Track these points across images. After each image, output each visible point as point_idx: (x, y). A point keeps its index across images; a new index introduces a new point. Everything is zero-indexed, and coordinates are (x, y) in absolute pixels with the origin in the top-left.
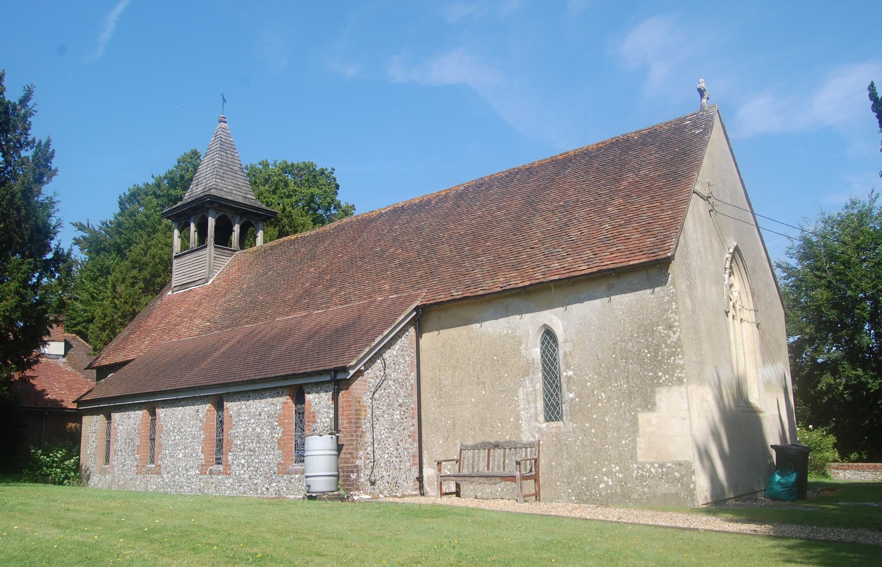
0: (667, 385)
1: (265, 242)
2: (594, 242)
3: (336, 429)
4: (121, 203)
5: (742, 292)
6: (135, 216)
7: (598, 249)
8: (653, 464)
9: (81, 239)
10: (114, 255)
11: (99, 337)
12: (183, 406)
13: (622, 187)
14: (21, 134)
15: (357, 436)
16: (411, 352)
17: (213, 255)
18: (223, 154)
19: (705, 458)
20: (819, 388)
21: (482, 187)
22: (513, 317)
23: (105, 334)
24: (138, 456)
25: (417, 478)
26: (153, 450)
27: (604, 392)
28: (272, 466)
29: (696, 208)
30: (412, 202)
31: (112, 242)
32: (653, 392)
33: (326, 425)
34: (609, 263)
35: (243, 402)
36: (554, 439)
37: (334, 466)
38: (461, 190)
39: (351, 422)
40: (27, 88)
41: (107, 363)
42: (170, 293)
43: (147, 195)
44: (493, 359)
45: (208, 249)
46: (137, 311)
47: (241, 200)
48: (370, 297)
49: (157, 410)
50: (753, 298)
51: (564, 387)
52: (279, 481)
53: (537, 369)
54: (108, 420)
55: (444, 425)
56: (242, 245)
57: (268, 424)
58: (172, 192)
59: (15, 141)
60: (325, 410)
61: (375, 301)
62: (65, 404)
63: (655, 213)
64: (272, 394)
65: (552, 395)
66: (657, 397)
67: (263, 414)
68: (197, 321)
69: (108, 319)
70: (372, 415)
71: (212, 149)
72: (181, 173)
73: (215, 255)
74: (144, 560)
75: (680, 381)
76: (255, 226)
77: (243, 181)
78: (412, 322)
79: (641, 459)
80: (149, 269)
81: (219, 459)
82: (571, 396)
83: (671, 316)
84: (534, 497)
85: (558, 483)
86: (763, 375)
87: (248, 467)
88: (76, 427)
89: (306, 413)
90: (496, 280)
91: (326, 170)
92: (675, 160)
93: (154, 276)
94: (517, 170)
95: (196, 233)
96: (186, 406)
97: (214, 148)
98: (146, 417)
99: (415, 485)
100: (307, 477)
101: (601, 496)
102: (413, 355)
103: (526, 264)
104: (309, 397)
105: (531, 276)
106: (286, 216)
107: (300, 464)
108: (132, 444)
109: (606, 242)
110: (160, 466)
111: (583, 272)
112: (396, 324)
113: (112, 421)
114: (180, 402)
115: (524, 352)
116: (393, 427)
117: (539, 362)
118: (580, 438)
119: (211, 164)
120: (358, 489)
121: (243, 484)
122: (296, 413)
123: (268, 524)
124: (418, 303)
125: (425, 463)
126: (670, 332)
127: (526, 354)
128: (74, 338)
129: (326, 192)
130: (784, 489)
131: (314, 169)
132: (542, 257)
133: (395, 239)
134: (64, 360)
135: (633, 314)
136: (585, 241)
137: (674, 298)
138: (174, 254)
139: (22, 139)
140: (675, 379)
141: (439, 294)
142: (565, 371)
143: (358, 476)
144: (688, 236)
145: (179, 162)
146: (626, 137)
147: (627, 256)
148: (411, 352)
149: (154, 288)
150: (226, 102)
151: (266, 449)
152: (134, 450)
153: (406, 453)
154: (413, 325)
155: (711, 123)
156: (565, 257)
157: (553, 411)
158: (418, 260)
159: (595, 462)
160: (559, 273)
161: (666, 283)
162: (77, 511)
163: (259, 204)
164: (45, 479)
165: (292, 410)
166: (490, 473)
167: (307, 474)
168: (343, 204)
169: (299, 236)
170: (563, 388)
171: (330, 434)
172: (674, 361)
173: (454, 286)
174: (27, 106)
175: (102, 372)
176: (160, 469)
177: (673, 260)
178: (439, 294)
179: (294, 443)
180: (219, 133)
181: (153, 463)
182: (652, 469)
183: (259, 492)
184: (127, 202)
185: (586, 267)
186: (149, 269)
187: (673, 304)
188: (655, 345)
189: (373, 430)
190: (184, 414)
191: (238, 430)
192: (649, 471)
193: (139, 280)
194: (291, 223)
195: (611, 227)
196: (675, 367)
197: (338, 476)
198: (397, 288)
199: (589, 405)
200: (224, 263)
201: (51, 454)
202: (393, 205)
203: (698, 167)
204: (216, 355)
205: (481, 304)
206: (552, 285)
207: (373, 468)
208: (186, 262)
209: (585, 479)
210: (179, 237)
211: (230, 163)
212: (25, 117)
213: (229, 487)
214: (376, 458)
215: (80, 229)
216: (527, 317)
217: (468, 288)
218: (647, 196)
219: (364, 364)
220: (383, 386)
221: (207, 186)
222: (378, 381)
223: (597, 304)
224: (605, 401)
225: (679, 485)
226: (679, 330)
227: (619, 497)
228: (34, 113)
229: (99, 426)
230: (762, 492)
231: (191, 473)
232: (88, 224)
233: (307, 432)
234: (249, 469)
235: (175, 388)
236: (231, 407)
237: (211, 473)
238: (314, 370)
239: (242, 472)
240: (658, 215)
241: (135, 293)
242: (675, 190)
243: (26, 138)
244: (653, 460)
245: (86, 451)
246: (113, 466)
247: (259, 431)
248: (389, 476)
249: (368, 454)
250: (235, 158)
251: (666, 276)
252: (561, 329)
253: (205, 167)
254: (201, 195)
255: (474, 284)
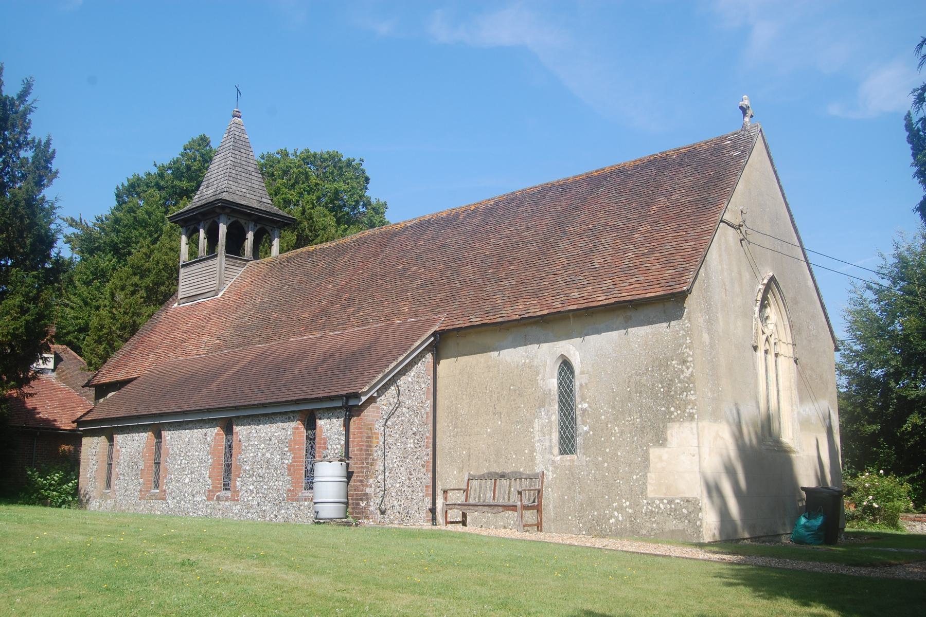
0: (679, 421)
1: (281, 251)
2: (616, 271)
3: (346, 456)
4: (118, 196)
5: (778, 324)
6: (134, 212)
7: (618, 279)
8: (662, 500)
9: (73, 236)
10: (109, 256)
11: (95, 351)
12: (190, 429)
13: (652, 212)
14: (20, 133)
15: (367, 463)
16: (427, 379)
17: (224, 265)
18: (236, 152)
19: (715, 494)
20: (904, 429)
21: (513, 202)
22: (531, 346)
23: (102, 347)
24: (141, 481)
25: (429, 509)
26: (158, 474)
27: (618, 426)
28: (281, 492)
29: (724, 238)
30: (439, 215)
31: (108, 240)
32: (665, 427)
33: (336, 452)
34: (626, 294)
35: (253, 427)
36: (567, 472)
37: (343, 493)
38: (491, 205)
39: (361, 450)
40: (26, 82)
41: (108, 381)
42: (176, 305)
43: (148, 187)
44: (510, 389)
45: (218, 258)
46: (138, 322)
47: (255, 205)
48: (389, 320)
49: (162, 432)
50: (791, 331)
51: (579, 419)
52: (288, 508)
53: (553, 400)
54: (109, 442)
55: (460, 455)
56: (256, 255)
57: (278, 449)
58: (177, 183)
59: (13, 140)
60: (336, 436)
61: (393, 324)
62: (58, 424)
63: (679, 242)
64: (283, 419)
65: (567, 428)
66: (669, 432)
67: (273, 439)
68: (206, 339)
69: (105, 331)
70: (384, 443)
71: (225, 146)
72: (187, 163)
73: (226, 266)
74: (166, 555)
75: (691, 417)
76: (270, 232)
77: (258, 183)
78: (429, 348)
79: (651, 495)
80: (152, 277)
81: (226, 484)
82: (585, 428)
83: (685, 350)
84: (536, 527)
85: (570, 518)
86: (799, 413)
87: (257, 493)
88: (69, 450)
89: (317, 440)
90: (516, 307)
91: (354, 160)
92: (708, 185)
93: (157, 284)
94: (550, 186)
95: (206, 240)
96: (193, 429)
97: (227, 145)
98: (150, 439)
99: (427, 516)
100: (315, 503)
101: (610, 531)
102: (429, 382)
103: (547, 291)
104: (320, 423)
105: (550, 304)
106: (306, 218)
107: (309, 491)
108: (135, 467)
109: (626, 272)
110: (165, 491)
111: (601, 303)
112: (412, 349)
113: (115, 443)
114: (187, 424)
115: (541, 383)
116: (406, 456)
117: (556, 393)
118: (593, 472)
119: (223, 164)
120: (367, 518)
121: (251, 511)
122: (307, 439)
123: (163, 209)
124: (436, 328)
125: (439, 494)
126: (683, 367)
127: (543, 384)
128: (64, 350)
129: (353, 188)
130: (809, 533)
131: (340, 160)
132: (564, 284)
133: (419, 256)
134: (54, 374)
135: (649, 347)
136: (606, 270)
137: (689, 332)
138: (181, 263)
139: (21, 139)
140: (686, 415)
141: (458, 319)
142: (580, 403)
143: (368, 504)
144: (710, 268)
145: (185, 149)
146: (664, 155)
147: (645, 288)
148: (427, 379)
149: (157, 297)
150: (240, 93)
151: (275, 475)
152: (137, 474)
153: (419, 483)
154: (430, 351)
155: (750, 145)
156: (585, 286)
157: (567, 444)
158: (440, 282)
159: (607, 497)
160: (578, 302)
161: (681, 317)
162: (94, 524)
163: (275, 209)
164: (43, 501)
165: (303, 436)
166: (495, 502)
167: (315, 500)
168: (373, 201)
169: (318, 248)
170: (578, 420)
171: (339, 461)
172: (686, 396)
173: (474, 312)
174: (26, 101)
175: (102, 390)
176: (165, 495)
177: (690, 293)
178: (458, 319)
179: (304, 469)
180: (232, 129)
181: (157, 488)
182: (661, 506)
183: (268, 519)
184: (126, 194)
185: (605, 297)
186: (152, 277)
187: (688, 338)
188: (669, 379)
189: (385, 458)
190: (192, 437)
191: (247, 455)
192: (658, 507)
193: (140, 287)
194: (311, 226)
195: (634, 256)
196: (687, 403)
197: (347, 504)
198: (417, 311)
199: (603, 439)
200: (236, 274)
201: (48, 477)
202: (420, 218)
203: (730, 195)
204: (226, 376)
205: (499, 331)
206: (571, 314)
207: (383, 497)
208: (194, 272)
209: (596, 513)
210: (187, 244)
211: (244, 163)
212: (25, 114)
213: (236, 514)
214: (387, 487)
215: (71, 225)
216: (545, 346)
217: (487, 315)
218: (675, 224)
219: (377, 391)
220: (397, 413)
221: (219, 188)
222: (391, 408)
223: (614, 335)
224: (618, 435)
225: (686, 521)
226: (692, 365)
227: (628, 533)
228: (34, 109)
229: (100, 448)
230: (788, 536)
231: (198, 499)
232: (81, 219)
233: (317, 458)
234: (258, 495)
235: (182, 410)
236: (240, 431)
237: (218, 499)
238: (325, 395)
239: (251, 498)
240: (681, 245)
241: (136, 303)
242: (702, 219)
243: (26, 137)
244: (662, 496)
245: (86, 475)
246: (114, 491)
247: (269, 457)
248: (400, 505)
249: (378, 482)
250: (250, 157)
251: (682, 309)
252: (578, 360)
253: (217, 167)
254: (212, 199)
255: (494, 311)
